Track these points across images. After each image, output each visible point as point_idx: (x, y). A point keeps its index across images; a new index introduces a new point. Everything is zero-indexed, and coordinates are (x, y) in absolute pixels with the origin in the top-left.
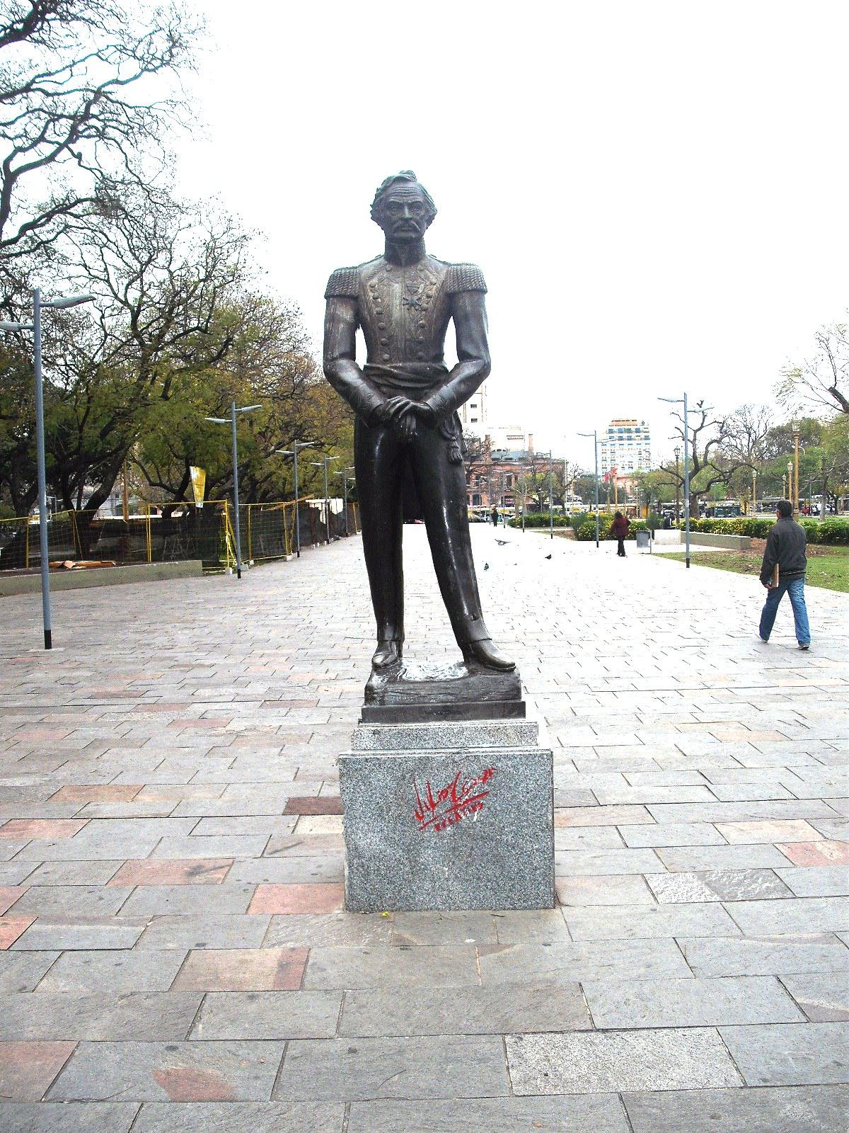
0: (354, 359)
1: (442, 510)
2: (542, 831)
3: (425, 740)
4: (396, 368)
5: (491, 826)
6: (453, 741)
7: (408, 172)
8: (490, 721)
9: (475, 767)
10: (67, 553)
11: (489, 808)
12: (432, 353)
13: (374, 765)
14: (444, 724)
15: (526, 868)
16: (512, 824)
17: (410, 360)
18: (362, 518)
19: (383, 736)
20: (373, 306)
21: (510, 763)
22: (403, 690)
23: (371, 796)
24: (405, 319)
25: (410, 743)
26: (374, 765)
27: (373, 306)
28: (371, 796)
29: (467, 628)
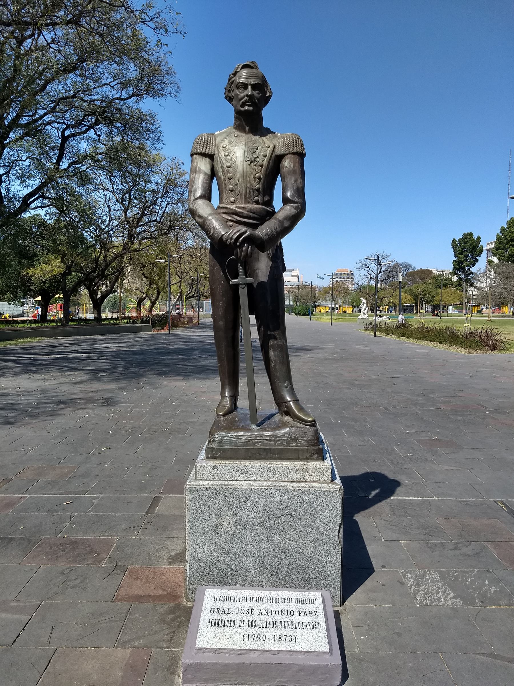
0: (210, 201)
1: (242, 240)
2: (334, 548)
3: (250, 474)
4: (239, 208)
5: (296, 542)
6: (270, 476)
7: (252, 62)
8: (296, 463)
9: (286, 497)
10: (20, 326)
11: (295, 529)
12: (266, 198)
13: (212, 493)
14: (265, 464)
15: (321, 575)
16: (311, 542)
17: (249, 203)
18: (287, 660)
19: (219, 470)
20: (224, 161)
21: (311, 496)
22: (236, 436)
23: (209, 516)
24: (247, 172)
25: (239, 476)
26: (212, 493)
27: (224, 161)
28: (209, 516)
29: (207, 180)
